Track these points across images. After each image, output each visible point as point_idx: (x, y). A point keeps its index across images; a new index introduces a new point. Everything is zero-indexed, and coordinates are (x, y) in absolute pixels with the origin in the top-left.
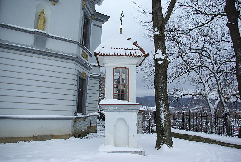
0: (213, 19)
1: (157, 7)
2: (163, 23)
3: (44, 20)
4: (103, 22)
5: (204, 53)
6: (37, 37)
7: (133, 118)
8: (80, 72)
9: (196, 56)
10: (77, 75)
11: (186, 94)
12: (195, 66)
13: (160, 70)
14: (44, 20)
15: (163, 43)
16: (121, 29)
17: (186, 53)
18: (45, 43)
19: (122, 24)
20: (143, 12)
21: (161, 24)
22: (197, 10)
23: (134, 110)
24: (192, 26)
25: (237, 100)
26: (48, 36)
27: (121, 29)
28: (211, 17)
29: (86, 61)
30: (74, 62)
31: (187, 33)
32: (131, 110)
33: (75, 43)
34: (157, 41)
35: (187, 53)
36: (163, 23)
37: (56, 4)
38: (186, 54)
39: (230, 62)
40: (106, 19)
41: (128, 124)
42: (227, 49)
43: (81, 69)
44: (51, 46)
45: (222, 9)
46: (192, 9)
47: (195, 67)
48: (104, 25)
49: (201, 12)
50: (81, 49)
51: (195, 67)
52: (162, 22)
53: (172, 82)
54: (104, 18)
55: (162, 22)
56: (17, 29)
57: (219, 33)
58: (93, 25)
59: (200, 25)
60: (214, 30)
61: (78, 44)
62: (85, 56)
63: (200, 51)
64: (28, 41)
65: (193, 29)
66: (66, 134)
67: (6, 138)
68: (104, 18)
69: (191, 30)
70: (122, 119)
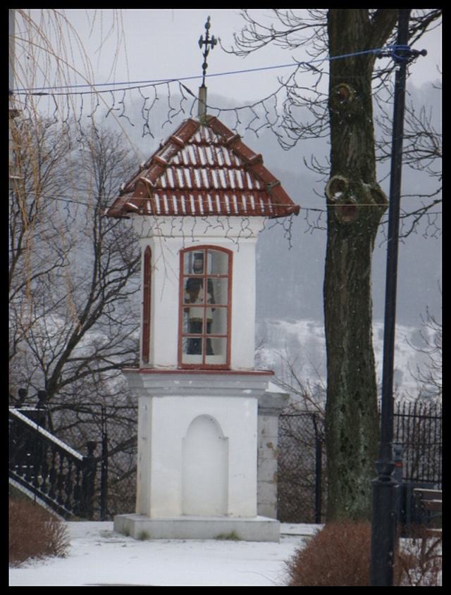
15: (363, 134)
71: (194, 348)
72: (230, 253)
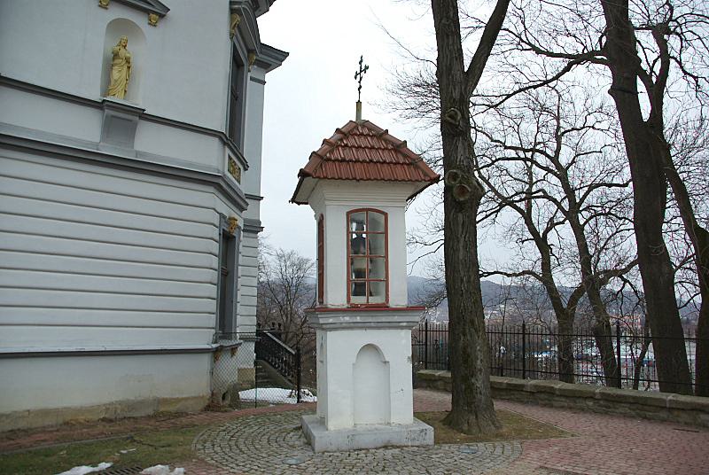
0: (567, 69)
1: (451, 47)
2: (465, 89)
3: (129, 68)
4: (268, 67)
5: (540, 159)
6: (113, 116)
7: (398, 346)
8: (224, 217)
9: (516, 167)
10: (218, 224)
11: (489, 274)
12: (517, 194)
13: (460, 215)
14: (129, 68)
16: (359, 103)
17: (494, 159)
18: (131, 132)
19: (358, 85)
20: (408, 54)
21: (461, 94)
22: (521, 39)
23: (405, 324)
24: (511, 86)
25: (623, 287)
26: (142, 115)
27: (359, 103)
28: (561, 64)
29: (237, 183)
30: (211, 189)
31: (498, 105)
32: (397, 324)
33: (215, 136)
34: (451, 136)
35: (497, 160)
36: (465, 89)
37: (161, 24)
38: (493, 162)
39: (610, 185)
40: (276, 58)
41: (387, 360)
42: (601, 152)
43: (227, 209)
44: (151, 144)
45: (594, 41)
46: (507, 37)
47: (517, 198)
48: (270, 77)
49: (533, 48)
50: (228, 151)
51: (517, 198)
52: (463, 88)
53: (214, 209)
54: (276, 57)
55: (463, 88)
56: (15, 84)
57: (579, 107)
58: (252, 79)
59: (531, 84)
60: (566, 97)
61: (221, 139)
62: (234, 169)
63: (529, 155)
64: (83, 129)
65: (515, 93)
66: (193, 395)
67: (29, 411)
68: (276, 57)
69: (509, 96)
70: (371, 348)
71: (356, 294)
72: (386, 215)
